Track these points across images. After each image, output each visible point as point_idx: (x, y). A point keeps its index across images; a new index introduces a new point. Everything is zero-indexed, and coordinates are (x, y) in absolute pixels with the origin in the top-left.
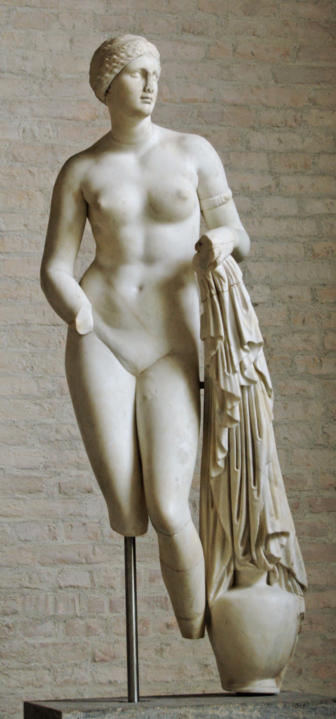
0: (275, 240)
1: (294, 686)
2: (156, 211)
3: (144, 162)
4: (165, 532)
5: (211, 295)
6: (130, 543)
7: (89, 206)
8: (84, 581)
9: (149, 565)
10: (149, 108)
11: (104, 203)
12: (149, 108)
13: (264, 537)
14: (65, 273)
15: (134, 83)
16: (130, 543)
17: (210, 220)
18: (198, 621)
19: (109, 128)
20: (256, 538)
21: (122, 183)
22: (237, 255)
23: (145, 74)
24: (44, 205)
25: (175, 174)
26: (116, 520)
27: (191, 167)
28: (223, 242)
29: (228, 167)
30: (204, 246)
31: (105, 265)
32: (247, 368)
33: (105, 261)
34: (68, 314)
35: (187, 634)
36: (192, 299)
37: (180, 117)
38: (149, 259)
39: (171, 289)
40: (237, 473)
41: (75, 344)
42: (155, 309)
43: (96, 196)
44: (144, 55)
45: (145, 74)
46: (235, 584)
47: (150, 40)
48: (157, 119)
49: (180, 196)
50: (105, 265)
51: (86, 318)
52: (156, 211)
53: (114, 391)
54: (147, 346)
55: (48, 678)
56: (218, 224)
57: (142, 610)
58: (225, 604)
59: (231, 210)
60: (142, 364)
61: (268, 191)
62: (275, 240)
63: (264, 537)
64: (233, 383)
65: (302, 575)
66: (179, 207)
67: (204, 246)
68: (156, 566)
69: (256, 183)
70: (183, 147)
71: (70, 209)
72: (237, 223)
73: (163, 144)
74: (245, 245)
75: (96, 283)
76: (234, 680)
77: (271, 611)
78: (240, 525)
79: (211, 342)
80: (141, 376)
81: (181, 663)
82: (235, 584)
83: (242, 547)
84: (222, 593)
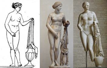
0: (101, 22)
1: (103, 66)
2: (89, 19)
3: (88, 14)
4: (90, 51)
5: (94, 27)
6: (86, 52)
7: (82, 19)
8: (82, 56)
9: (88, 54)
10: (88, 9)
11: (84, 18)
12: (88, 9)
13: (100, 51)
14: (80, 25)
15: (87, 6)
16: (86, 52)
17: (94, 20)
18: (93, 60)
19: (84, 11)
20: (99, 52)
21: (86, 16)
22: (97, 23)
23: (88, 6)
24: (78, 18)
25: (91, 16)
26: (85, 50)
27: (92, 15)
28: (96, 22)
29: (96, 15)
30: (94, 23)
31: (84, 25)
32: (98, 35)
33: (84, 24)
34: (80, 29)
35: (92, 61)
36: (93, 28)
37: (91, 10)
38: (88, 24)
39: (90, 27)
40: (97, 45)
41: (81, 32)
42: (89, 29)
43: (83, 18)
44: (88, 4)
45: (88, 6)
46: (97, 56)
47: (88, 2)
48: (89, 10)
49: (91, 18)
50: (84, 25)
51: (82, 30)
52: (89, 19)
53: (85, 37)
54: (88, 33)
55: (78, 65)
56: (95, 20)
57: (88, 59)
58: (96, 58)
59: (96, 19)
60: (87, 34)
61: (100, 17)
62: (101, 22)
63: (100, 51)
64: (97, 36)
65: (103, 55)
66: (91, 19)
67: (94, 23)
68: (89, 54)
69: (99, 16)
70: (92, 13)
71: (80, 19)
72: (97, 20)
73: (89, 58)
74: (98, 23)
75: (83, 26)
76: (97, 65)
77: (100, 59)
78: (97, 50)
79: (94, 32)
80: (87, 36)
81: (92, 64)
82: (97, 56)
83: (98, 53)
84: (96, 57)
